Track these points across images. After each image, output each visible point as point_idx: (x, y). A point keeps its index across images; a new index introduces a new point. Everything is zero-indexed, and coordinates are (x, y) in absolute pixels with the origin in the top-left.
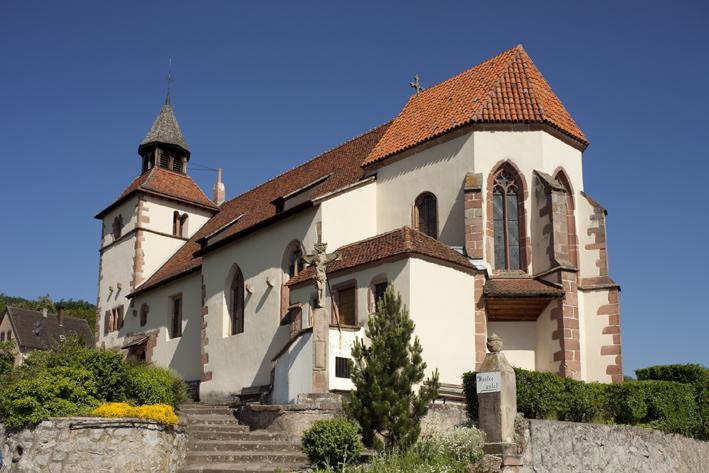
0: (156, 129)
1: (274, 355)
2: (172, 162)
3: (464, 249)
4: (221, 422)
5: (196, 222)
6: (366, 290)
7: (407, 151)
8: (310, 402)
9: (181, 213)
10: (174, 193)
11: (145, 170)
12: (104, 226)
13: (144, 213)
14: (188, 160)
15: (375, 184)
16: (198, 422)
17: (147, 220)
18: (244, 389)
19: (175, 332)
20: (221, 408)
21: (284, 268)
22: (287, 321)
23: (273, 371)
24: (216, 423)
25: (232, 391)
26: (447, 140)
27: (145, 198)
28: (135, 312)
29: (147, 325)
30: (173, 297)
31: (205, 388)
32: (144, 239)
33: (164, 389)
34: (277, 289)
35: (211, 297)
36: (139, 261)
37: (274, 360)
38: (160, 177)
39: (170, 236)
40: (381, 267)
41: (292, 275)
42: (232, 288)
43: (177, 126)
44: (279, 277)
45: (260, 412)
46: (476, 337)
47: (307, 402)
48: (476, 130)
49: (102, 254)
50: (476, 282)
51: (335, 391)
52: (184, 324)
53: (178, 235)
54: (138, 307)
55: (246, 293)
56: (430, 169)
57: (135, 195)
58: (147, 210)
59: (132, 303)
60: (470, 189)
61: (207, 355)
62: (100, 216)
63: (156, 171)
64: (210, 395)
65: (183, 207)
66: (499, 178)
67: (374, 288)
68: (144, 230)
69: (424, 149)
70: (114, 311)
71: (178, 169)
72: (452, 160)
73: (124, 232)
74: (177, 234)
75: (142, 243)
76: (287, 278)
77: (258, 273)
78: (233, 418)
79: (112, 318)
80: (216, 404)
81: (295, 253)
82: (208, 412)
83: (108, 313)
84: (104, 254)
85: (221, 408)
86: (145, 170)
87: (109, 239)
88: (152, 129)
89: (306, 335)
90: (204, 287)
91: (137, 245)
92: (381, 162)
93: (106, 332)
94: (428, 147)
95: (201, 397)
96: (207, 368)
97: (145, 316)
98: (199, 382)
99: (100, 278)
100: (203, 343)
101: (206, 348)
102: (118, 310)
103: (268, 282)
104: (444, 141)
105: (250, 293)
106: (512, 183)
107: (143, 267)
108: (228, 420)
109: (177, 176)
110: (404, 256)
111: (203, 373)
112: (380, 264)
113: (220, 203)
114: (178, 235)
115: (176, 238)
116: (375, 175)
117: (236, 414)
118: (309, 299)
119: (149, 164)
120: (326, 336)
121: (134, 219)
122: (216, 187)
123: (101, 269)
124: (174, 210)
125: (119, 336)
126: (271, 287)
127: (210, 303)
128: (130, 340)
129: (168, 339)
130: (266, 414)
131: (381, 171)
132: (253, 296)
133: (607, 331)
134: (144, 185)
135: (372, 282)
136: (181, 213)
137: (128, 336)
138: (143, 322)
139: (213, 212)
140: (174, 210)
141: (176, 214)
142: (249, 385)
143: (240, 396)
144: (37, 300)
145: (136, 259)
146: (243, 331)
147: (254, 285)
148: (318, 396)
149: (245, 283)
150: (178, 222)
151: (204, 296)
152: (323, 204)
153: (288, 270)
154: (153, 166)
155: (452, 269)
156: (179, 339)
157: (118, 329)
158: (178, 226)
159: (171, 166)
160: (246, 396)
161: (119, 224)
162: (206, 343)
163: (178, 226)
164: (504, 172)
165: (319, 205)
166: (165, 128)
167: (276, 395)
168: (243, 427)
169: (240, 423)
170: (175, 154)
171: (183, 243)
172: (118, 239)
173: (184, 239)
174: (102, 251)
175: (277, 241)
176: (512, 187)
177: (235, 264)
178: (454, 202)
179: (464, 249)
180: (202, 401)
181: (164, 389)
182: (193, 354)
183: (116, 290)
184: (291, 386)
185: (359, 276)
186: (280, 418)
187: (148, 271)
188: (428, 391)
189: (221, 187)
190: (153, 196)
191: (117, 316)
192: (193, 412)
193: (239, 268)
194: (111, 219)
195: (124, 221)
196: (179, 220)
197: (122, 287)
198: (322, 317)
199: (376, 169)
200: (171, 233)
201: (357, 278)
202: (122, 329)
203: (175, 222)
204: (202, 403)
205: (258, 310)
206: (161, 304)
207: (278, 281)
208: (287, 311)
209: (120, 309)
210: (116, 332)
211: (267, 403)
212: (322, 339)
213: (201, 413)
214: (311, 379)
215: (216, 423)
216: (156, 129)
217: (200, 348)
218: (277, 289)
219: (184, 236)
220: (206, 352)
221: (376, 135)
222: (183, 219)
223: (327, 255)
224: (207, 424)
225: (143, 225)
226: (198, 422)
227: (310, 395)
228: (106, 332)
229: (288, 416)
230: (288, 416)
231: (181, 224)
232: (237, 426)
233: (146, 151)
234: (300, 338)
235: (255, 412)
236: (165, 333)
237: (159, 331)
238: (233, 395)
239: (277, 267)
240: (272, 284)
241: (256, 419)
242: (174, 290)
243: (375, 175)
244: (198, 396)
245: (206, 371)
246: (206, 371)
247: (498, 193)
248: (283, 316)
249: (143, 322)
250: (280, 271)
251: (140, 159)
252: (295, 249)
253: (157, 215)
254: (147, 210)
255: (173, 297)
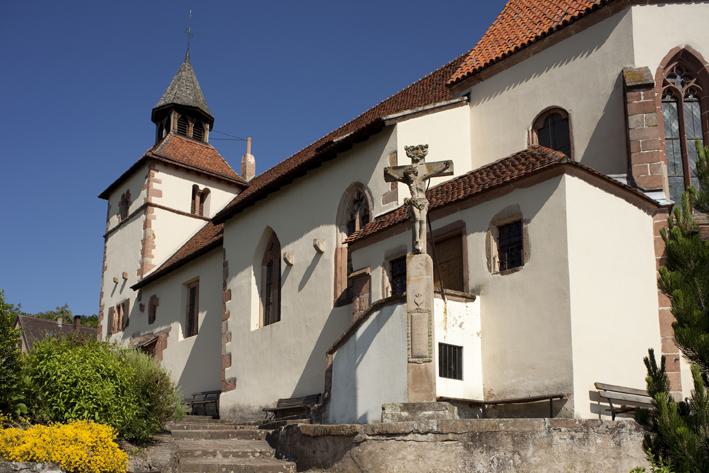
0: (172, 89)
1: (331, 345)
2: (191, 129)
3: (630, 178)
4: (245, 455)
5: (220, 199)
6: (483, 235)
7: (519, 54)
8: (407, 419)
9: (202, 187)
10: (193, 164)
11: (160, 139)
12: (109, 207)
13: (155, 186)
14: (211, 128)
15: (467, 108)
16: (205, 453)
17: (159, 194)
18: (280, 401)
19: (190, 329)
20: (247, 429)
21: (339, 225)
22: (344, 300)
23: (329, 371)
24: (236, 455)
25: (264, 405)
26: (584, 27)
27: (157, 167)
28: (142, 307)
29: (156, 321)
30: (188, 285)
31: (226, 400)
32: (155, 218)
33: (110, 387)
34: (329, 256)
35: (236, 275)
36: (149, 244)
37: (331, 352)
38: (175, 144)
39: (187, 215)
40: (511, 195)
41: (350, 229)
42: (263, 264)
43: (198, 87)
44: (332, 238)
45: (316, 437)
46: (660, 312)
47: (401, 419)
48: (635, 4)
49: (106, 241)
50: (656, 226)
51: (441, 399)
52: (201, 317)
53: (197, 213)
54: (146, 301)
55: (284, 265)
56: (557, 73)
57: (148, 163)
58: (159, 182)
59: (140, 295)
60: (628, 87)
61: (230, 355)
62: (106, 195)
63: (170, 137)
64: (234, 410)
65: (204, 181)
66: (672, 76)
67: (496, 231)
68: (156, 206)
69: (548, 46)
70: (118, 308)
71: (198, 136)
72: (595, 54)
73: (132, 210)
74: (196, 212)
75: (153, 221)
76: (344, 236)
77: (301, 236)
78: (265, 447)
79: (116, 316)
80: (241, 425)
81: (355, 202)
82: (225, 436)
83: (111, 311)
84: (110, 240)
85: (247, 429)
86: (160, 139)
87: (115, 220)
88: (168, 91)
89: (386, 309)
90: (225, 265)
91: (146, 225)
92: (476, 75)
93: (110, 334)
94: (552, 43)
95: (221, 414)
96: (229, 373)
97: (155, 312)
98: (220, 392)
99: (104, 268)
100: (224, 339)
101: (229, 346)
102: (123, 305)
103: (316, 247)
104: (577, 31)
105: (290, 265)
106: (692, 83)
107: (153, 252)
108: (257, 450)
109: (198, 145)
110: (561, 173)
111: (224, 381)
112: (508, 192)
113: (249, 179)
114: (197, 213)
115: (196, 217)
116: (468, 95)
117: (272, 440)
118: (382, 260)
119: (164, 131)
120: (429, 304)
121: (144, 193)
122: (245, 159)
123: (105, 257)
124: (193, 183)
125: (124, 338)
126: (320, 252)
127: (233, 284)
128: (137, 341)
129: (181, 337)
130: (329, 441)
131: (476, 89)
132: (294, 267)
133: (365, 416)
134: (155, 152)
135: (493, 223)
136: (202, 187)
137: (134, 336)
138: (152, 319)
139: (239, 186)
140: (193, 183)
141: (195, 188)
142: (288, 395)
143: (275, 411)
144: (55, 311)
145: (144, 242)
146: (279, 320)
147: (296, 253)
148: (422, 407)
149: (283, 252)
150: (198, 198)
151: (226, 276)
152: (400, 125)
153: (345, 227)
154: (168, 132)
155: (623, 201)
156: (195, 337)
157: (123, 329)
158: (198, 204)
159: (191, 133)
160: (284, 410)
161: (126, 202)
162: (229, 339)
163: (198, 204)
164: (678, 67)
165: (393, 127)
166: (185, 89)
167: (335, 408)
168: (284, 463)
169: (278, 457)
170: (195, 119)
171: (201, 224)
172: (125, 220)
173: (205, 219)
174: (106, 237)
175: (332, 186)
176: (692, 90)
177: (268, 227)
178: (600, 115)
179: (630, 178)
180: (222, 418)
181: (110, 387)
182: (212, 357)
183: (121, 281)
184: (361, 393)
185: (465, 215)
186: (357, 450)
187: (159, 258)
188: (653, 403)
189: (251, 159)
190: (166, 165)
191: (122, 313)
192: (199, 436)
193: (274, 234)
194: (117, 198)
195: (132, 196)
196: (199, 196)
197: (128, 277)
198: (423, 268)
199: (469, 86)
200: (189, 212)
201: (465, 220)
202: (127, 329)
203: (194, 198)
204: (222, 422)
205: (301, 287)
206: (173, 295)
207: (330, 244)
208: (345, 286)
209: (125, 305)
210: (121, 334)
211: (319, 420)
212: (422, 307)
213: (213, 436)
214: (402, 378)
215: (236, 455)
216: (172, 89)
217: (219, 346)
218: (329, 256)
219: (205, 215)
220: (228, 351)
221: (454, 67)
222: (204, 195)
223: (428, 164)
224: (220, 456)
225: (154, 200)
226: (205, 453)
227: (406, 407)
228: (110, 334)
229: (373, 446)
230: (373, 446)
231: (202, 201)
232: (272, 462)
233: (161, 116)
234: (375, 315)
235: (307, 438)
236: (177, 330)
237: (170, 329)
238: (265, 410)
239: (328, 223)
240: (321, 248)
241: (308, 450)
242: (188, 276)
243: (468, 95)
244: (217, 411)
245: (228, 376)
246: (228, 376)
247: (668, 98)
248: (339, 294)
249: (152, 319)
250: (334, 228)
251: (153, 127)
252: (355, 196)
253: (171, 189)
254: (159, 182)
255: (188, 285)
